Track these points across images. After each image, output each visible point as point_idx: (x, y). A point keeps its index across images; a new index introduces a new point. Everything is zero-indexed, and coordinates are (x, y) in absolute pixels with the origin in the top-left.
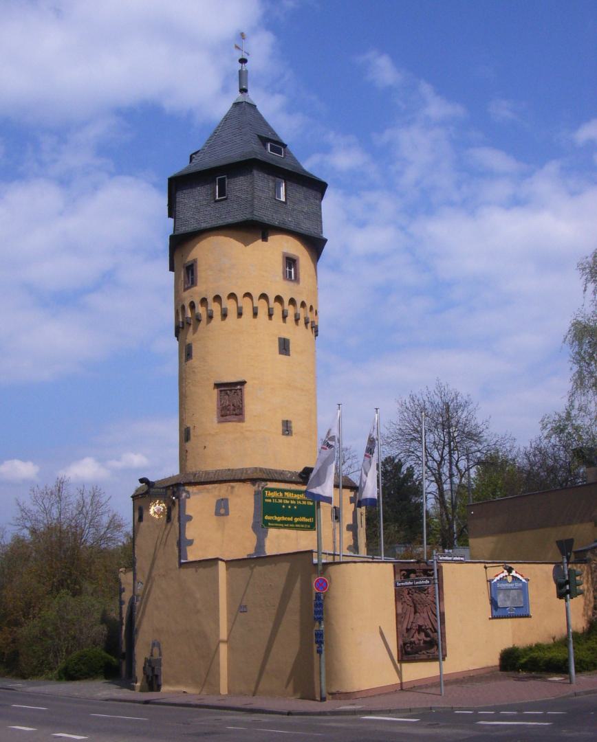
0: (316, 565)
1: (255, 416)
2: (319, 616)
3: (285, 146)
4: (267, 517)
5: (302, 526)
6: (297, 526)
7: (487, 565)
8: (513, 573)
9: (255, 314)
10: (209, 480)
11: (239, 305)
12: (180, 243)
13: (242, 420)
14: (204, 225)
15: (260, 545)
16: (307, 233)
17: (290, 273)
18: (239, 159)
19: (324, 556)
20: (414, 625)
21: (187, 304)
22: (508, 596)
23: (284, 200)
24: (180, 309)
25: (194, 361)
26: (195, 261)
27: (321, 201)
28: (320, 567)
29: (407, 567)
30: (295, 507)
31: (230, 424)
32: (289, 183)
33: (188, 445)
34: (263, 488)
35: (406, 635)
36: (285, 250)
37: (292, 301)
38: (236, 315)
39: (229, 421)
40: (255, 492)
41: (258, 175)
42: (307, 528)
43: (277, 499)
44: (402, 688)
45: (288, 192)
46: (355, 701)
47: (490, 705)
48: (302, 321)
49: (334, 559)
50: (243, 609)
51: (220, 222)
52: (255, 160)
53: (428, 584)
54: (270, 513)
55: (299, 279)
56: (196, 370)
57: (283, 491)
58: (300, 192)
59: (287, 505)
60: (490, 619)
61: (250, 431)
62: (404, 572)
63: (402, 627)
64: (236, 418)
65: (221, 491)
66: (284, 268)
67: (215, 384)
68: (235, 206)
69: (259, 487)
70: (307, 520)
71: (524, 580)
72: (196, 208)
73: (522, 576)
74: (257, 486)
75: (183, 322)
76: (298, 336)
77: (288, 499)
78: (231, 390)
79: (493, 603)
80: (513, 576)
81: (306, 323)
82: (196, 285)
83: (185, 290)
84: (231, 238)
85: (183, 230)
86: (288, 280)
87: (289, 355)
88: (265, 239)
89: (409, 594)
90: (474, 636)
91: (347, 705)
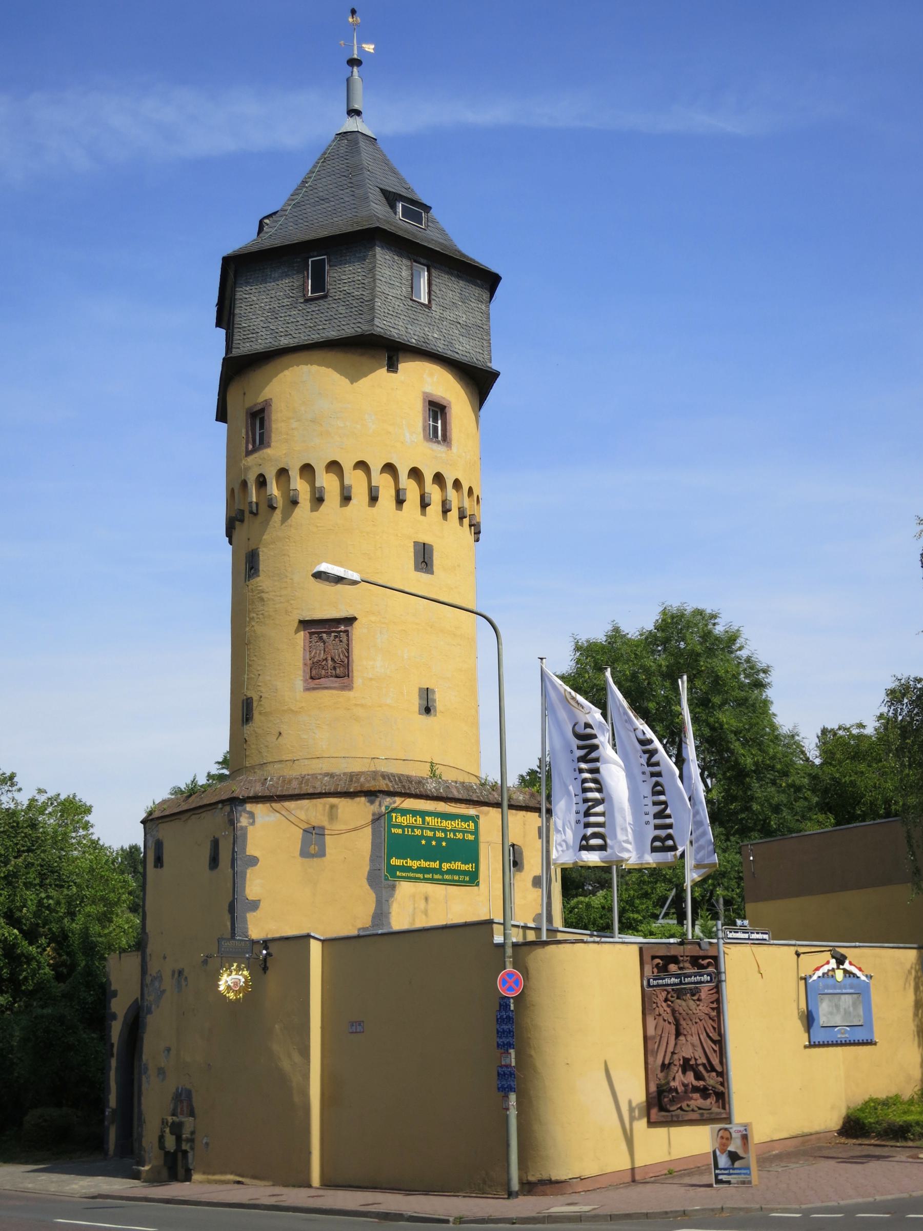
0: (502, 946)
1: (371, 679)
2: (506, 1041)
3: (427, 209)
4: (394, 861)
5: (456, 878)
6: (447, 877)
7: (801, 950)
8: (847, 966)
9: (373, 499)
10: (290, 792)
11: (346, 482)
12: (238, 368)
13: (348, 687)
14: (285, 342)
15: (381, 913)
16: (465, 359)
17: (435, 428)
18: (350, 229)
19: (514, 931)
20: (676, 1057)
21: (251, 479)
22: (837, 1007)
23: (426, 302)
24: (237, 489)
25: (263, 581)
26: (268, 403)
27: (488, 307)
28: (509, 951)
29: (662, 952)
30: (444, 844)
31: (326, 692)
32: (434, 273)
33: (248, 729)
34: (387, 807)
35: (661, 1075)
36: (429, 389)
37: (439, 479)
38: (366, 498)
39: (326, 688)
40: (374, 814)
41: (382, 257)
42: (464, 881)
43: (413, 828)
44: (634, 1177)
45: (434, 288)
46: (574, 1198)
47: (889, 1197)
48: (454, 514)
49: (525, 936)
50: (356, 1027)
51: (316, 337)
52: (378, 229)
53: (708, 982)
54: (397, 855)
55: (451, 440)
56: (264, 596)
57: (423, 814)
58: (452, 289)
59: (429, 839)
60: (806, 1047)
61: (362, 706)
62: (658, 961)
63: (655, 1061)
64: (336, 682)
65: (311, 812)
66: (425, 421)
67: (301, 622)
68: (342, 310)
69: (380, 805)
70: (464, 867)
71: (863, 978)
72: (272, 311)
73: (860, 969)
74: (377, 803)
75: (257, 504)
76: (449, 539)
77: (431, 829)
78: (329, 633)
79: (809, 1020)
80: (845, 971)
81: (462, 518)
82: (269, 446)
83: (248, 453)
84: (328, 367)
85: (244, 348)
86: (430, 440)
87: (432, 573)
88: (392, 367)
89: (666, 1000)
90: (784, 1083)
91: (562, 1205)
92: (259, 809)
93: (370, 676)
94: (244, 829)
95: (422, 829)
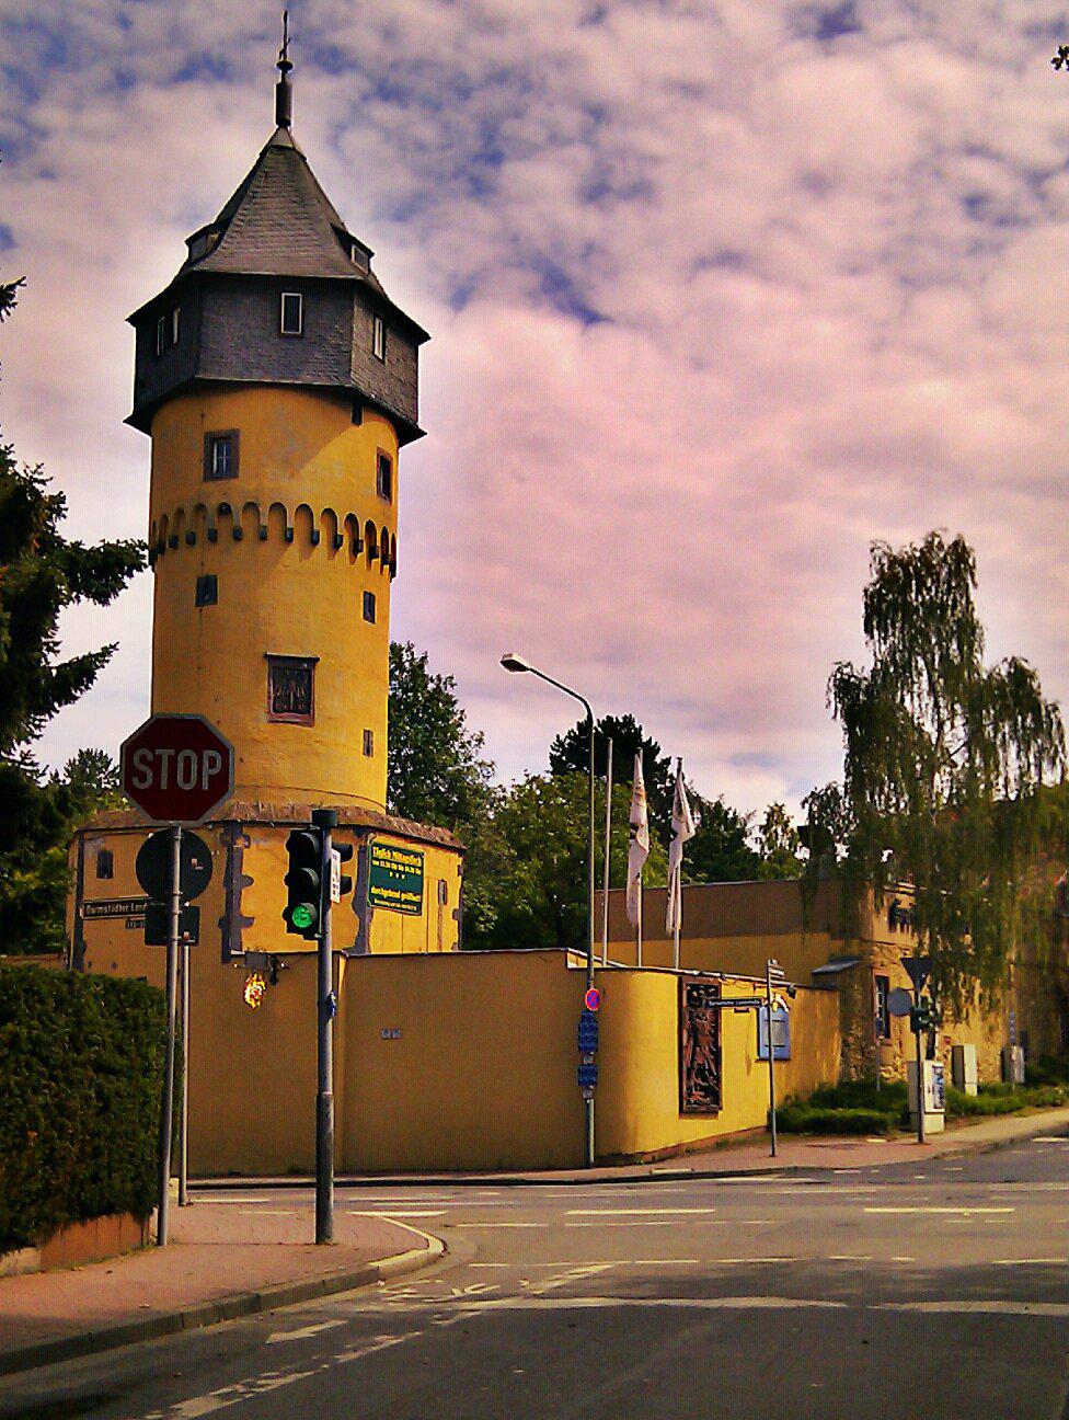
4: (374, 891)
6: (404, 906)
59: (395, 872)
92: (254, 833)
93: (330, 715)
94: (240, 851)
95: (391, 862)
